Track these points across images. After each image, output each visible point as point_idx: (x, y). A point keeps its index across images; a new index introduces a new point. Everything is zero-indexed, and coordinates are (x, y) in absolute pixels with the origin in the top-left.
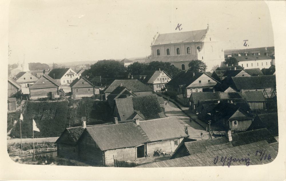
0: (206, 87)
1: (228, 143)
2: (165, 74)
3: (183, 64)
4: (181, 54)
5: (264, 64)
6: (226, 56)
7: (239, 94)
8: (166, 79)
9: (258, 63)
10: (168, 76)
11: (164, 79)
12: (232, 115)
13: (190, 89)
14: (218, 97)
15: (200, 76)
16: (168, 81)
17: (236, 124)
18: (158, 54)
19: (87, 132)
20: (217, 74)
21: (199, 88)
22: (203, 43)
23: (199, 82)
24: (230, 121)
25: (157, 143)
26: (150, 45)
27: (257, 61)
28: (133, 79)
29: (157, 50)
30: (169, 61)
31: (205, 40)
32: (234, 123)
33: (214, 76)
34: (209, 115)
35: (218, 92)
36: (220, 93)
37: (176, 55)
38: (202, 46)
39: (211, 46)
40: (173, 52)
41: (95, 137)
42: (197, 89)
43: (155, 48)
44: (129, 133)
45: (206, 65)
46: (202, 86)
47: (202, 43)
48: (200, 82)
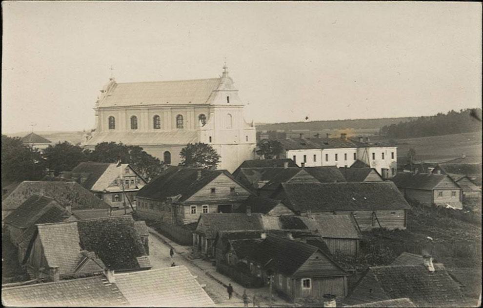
0: (225, 201)
2: (131, 172)
4: (163, 128)
5: (341, 157)
6: (258, 135)
7: (302, 221)
8: (132, 183)
10: (137, 177)
11: (130, 182)
12: (299, 266)
13: (191, 206)
14: (258, 225)
15: (215, 178)
16: (137, 188)
17: (308, 286)
20: (246, 176)
21: (211, 203)
23: (210, 191)
24: (296, 280)
26: (94, 105)
27: (326, 151)
28: (64, 180)
29: (108, 117)
30: (135, 142)
32: (304, 284)
33: (237, 175)
34: (245, 263)
36: (262, 216)
37: (153, 130)
39: (229, 114)
40: (145, 121)
42: (195, 207)
43: (105, 112)
45: (218, 153)
48: (213, 190)
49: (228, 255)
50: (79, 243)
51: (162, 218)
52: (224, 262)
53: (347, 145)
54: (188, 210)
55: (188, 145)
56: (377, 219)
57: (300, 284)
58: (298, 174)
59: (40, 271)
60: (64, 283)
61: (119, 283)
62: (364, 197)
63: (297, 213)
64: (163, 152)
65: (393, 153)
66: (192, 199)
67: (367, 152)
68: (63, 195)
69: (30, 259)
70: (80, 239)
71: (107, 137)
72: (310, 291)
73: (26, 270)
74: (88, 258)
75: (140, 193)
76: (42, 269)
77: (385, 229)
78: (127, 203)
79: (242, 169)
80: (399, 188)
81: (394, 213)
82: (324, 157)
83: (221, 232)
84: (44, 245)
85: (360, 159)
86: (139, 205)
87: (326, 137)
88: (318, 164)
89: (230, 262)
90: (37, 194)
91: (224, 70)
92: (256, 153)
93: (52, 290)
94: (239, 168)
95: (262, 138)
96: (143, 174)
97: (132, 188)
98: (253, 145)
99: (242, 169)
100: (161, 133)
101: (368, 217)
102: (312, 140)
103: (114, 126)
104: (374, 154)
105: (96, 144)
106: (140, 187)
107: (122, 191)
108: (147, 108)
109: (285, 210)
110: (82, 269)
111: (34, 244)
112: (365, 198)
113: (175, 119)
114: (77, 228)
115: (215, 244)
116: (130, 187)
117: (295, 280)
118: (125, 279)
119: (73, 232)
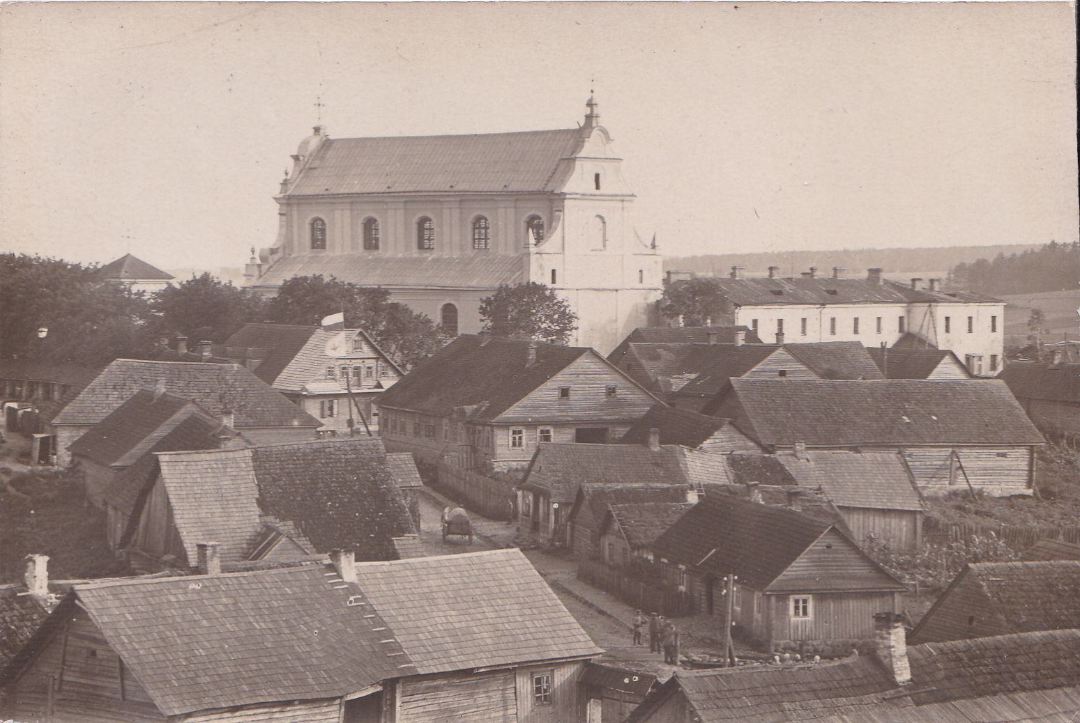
1: (892, 692)
2: (365, 348)
3: (447, 301)
5: (867, 327)
8: (369, 374)
9: (833, 320)
11: (363, 372)
14: (676, 473)
16: (379, 386)
18: (318, 242)
19: (81, 613)
20: (643, 362)
21: (559, 425)
22: (562, 197)
23: (557, 394)
25: (450, 685)
26: (276, 191)
27: (831, 311)
28: (210, 360)
31: (577, 182)
33: (621, 359)
35: (677, 448)
37: (415, 253)
38: (551, 213)
41: (128, 637)
42: (520, 432)
44: (306, 624)
45: (572, 309)
46: (575, 414)
47: (554, 199)
48: (565, 392)
49: (606, 541)
50: (257, 500)
51: (442, 457)
52: (597, 557)
53: (883, 296)
54: (503, 439)
55: (500, 289)
56: (961, 467)
57: (786, 609)
58: (769, 358)
59: (165, 563)
60: (237, 577)
61: (367, 583)
62: (930, 414)
63: (769, 449)
64: (440, 306)
65: (994, 318)
66: (511, 413)
67: (931, 313)
68: (209, 395)
69: (138, 536)
70: (260, 490)
71: (303, 267)
72: (808, 626)
73: (129, 561)
74: (279, 534)
75: (384, 400)
76: (169, 557)
77: (980, 493)
78: (355, 421)
79: (631, 344)
80: (1017, 398)
81: (1004, 455)
82: (828, 325)
83: (589, 487)
84: (173, 501)
85: (914, 329)
86: (386, 426)
87: (831, 277)
88: (812, 338)
89: (611, 556)
90: (149, 388)
91: (589, 109)
92: (661, 312)
93: (210, 592)
94: (625, 345)
95: (674, 278)
96: (394, 355)
97: (367, 386)
98: (653, 292)
99: (631, 344)
100: (436, 260)
101: (939, 463)
102: (797, 283)
103: (323, 241)
104: (947, 319)
105: (281, 283)
106: (388, 382)
107: (346, 392)
108: (403, 200)
109: (741, 440)
110: (402, 456)
111: (148, 500)
112: (934, 418)
113: (470, 226)
114: (251, 464)
115: (571, 517)
116: (364, 383)
117: (773, 599)
118: (379, 575)
119: (242, 473)
